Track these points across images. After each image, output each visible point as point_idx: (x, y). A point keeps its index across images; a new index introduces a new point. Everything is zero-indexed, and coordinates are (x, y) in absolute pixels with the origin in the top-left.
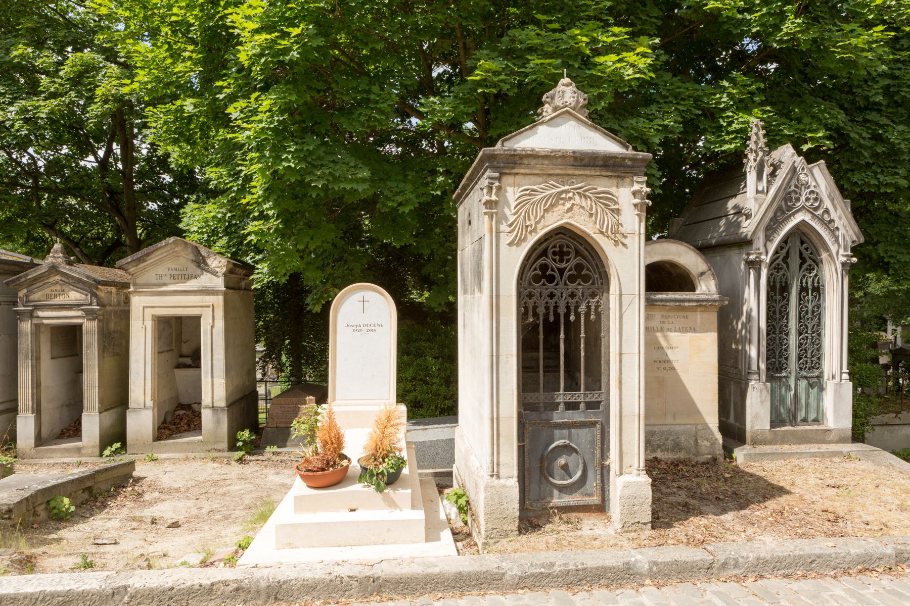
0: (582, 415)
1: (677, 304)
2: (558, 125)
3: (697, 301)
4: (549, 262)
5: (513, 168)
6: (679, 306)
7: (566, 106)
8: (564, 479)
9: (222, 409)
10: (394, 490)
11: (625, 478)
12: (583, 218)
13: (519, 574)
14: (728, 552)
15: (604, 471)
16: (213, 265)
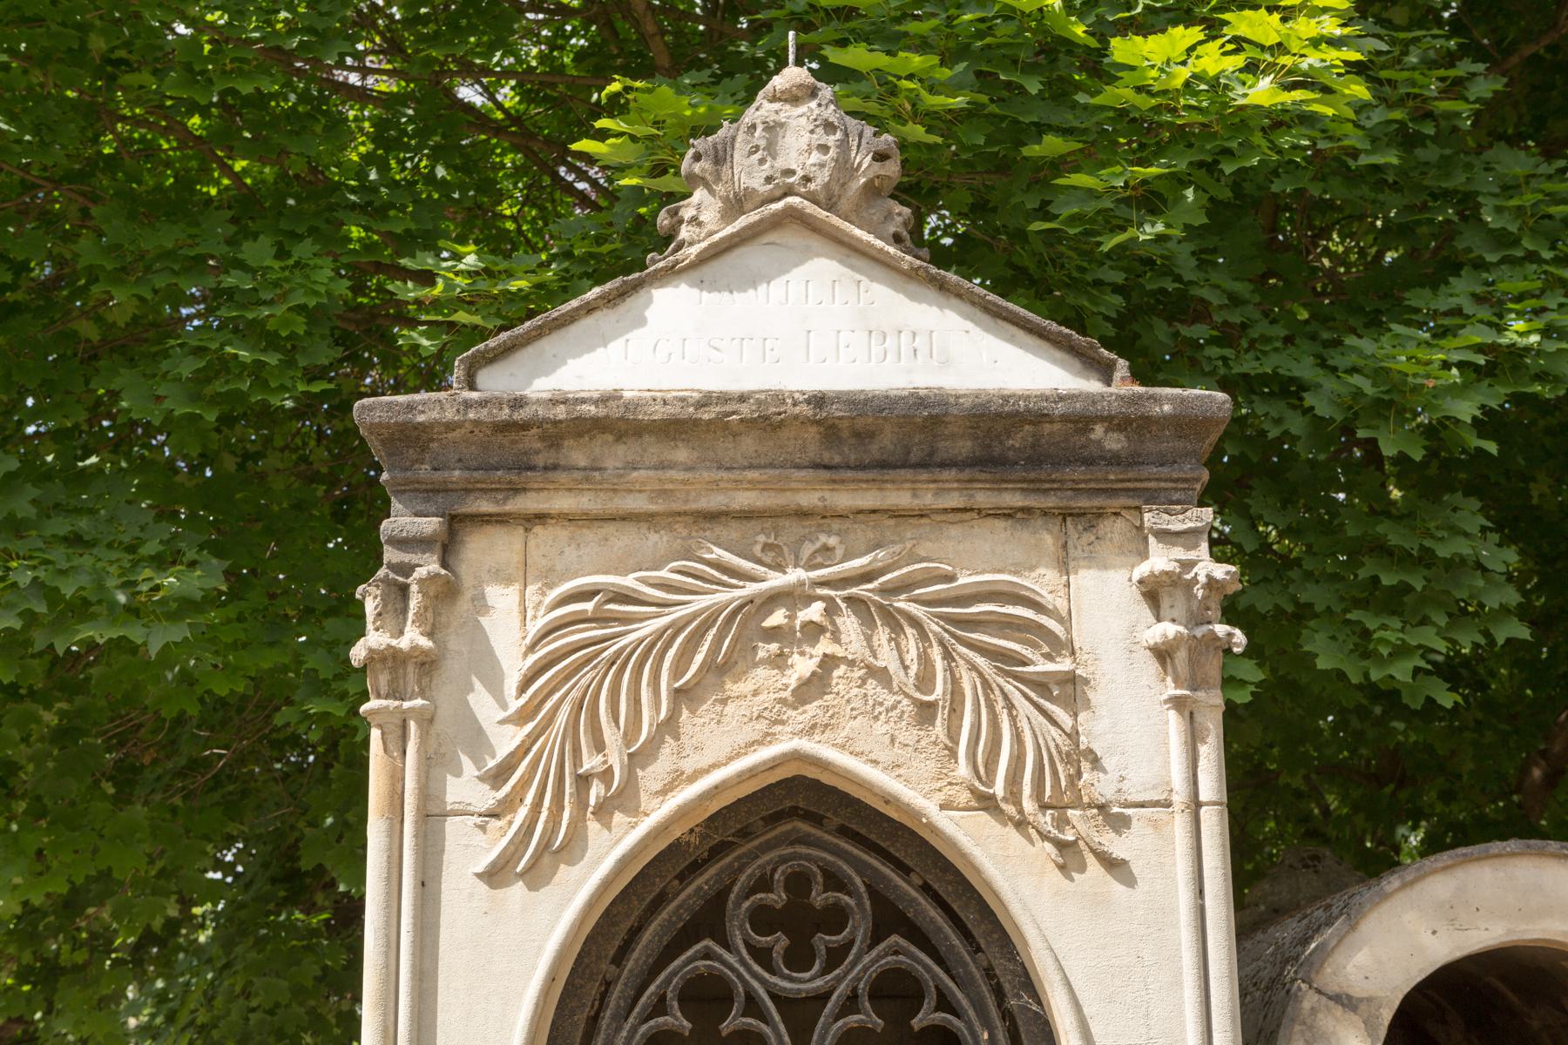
5: (516, 490)
7: (789, 191)
12: (880, 728)
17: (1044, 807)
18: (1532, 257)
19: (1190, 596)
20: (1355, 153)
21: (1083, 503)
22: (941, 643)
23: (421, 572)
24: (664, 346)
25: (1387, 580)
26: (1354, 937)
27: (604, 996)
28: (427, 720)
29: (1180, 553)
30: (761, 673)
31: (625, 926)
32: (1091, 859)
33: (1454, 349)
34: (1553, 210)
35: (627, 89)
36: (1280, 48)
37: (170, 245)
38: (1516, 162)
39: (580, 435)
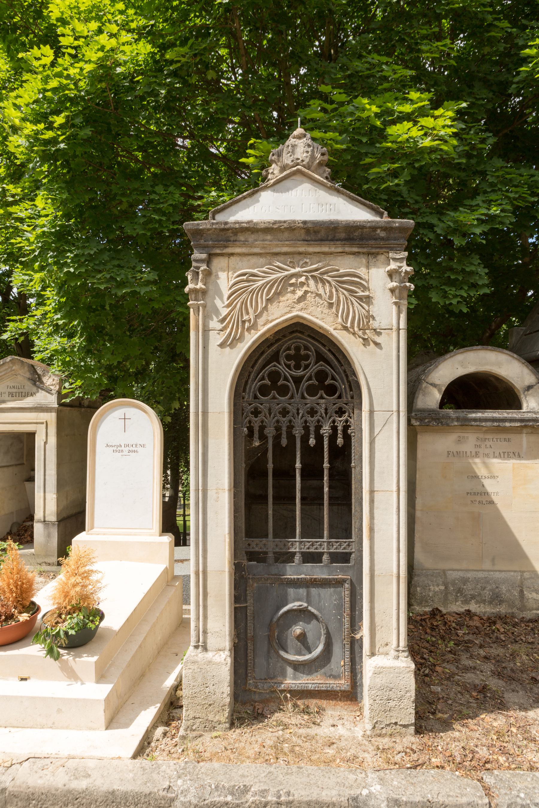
0: (325, 570)
1: (496, 424)
2: (287, 190)
3: (521, 420)
4: (281, 368)
5: (226, 247)
6: (499, 428)
7: (298, 164)
8: (300, 654)
9: (53, 523)
10: (75, 656)
11: (378, 661)
12: (319, 309)
13: (194, 801)
14: (514, 793)
15: (355, 646)
16: (48, 383)
17: (360, 330)
18: (500, 190)
19: (400, 275)
20: (454, 159)
21: (374, 250)
22: (335, 287)
23: (202, 268)
24: (265, 208)
25: (452, 277)
26: (437, 370)
27: (249, 376)
28: (204, 306)
29: (398, 264)
30: (289, 295)
31: (254, 359)
32: (371, 343)
33: (476, 215)
34: (507, 176)
35: (255, 142)
36: (434, 129)
37: (136, 187)
38: (499, 163)
39: (242, 232)
